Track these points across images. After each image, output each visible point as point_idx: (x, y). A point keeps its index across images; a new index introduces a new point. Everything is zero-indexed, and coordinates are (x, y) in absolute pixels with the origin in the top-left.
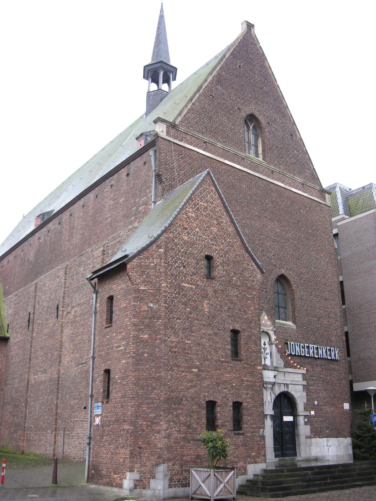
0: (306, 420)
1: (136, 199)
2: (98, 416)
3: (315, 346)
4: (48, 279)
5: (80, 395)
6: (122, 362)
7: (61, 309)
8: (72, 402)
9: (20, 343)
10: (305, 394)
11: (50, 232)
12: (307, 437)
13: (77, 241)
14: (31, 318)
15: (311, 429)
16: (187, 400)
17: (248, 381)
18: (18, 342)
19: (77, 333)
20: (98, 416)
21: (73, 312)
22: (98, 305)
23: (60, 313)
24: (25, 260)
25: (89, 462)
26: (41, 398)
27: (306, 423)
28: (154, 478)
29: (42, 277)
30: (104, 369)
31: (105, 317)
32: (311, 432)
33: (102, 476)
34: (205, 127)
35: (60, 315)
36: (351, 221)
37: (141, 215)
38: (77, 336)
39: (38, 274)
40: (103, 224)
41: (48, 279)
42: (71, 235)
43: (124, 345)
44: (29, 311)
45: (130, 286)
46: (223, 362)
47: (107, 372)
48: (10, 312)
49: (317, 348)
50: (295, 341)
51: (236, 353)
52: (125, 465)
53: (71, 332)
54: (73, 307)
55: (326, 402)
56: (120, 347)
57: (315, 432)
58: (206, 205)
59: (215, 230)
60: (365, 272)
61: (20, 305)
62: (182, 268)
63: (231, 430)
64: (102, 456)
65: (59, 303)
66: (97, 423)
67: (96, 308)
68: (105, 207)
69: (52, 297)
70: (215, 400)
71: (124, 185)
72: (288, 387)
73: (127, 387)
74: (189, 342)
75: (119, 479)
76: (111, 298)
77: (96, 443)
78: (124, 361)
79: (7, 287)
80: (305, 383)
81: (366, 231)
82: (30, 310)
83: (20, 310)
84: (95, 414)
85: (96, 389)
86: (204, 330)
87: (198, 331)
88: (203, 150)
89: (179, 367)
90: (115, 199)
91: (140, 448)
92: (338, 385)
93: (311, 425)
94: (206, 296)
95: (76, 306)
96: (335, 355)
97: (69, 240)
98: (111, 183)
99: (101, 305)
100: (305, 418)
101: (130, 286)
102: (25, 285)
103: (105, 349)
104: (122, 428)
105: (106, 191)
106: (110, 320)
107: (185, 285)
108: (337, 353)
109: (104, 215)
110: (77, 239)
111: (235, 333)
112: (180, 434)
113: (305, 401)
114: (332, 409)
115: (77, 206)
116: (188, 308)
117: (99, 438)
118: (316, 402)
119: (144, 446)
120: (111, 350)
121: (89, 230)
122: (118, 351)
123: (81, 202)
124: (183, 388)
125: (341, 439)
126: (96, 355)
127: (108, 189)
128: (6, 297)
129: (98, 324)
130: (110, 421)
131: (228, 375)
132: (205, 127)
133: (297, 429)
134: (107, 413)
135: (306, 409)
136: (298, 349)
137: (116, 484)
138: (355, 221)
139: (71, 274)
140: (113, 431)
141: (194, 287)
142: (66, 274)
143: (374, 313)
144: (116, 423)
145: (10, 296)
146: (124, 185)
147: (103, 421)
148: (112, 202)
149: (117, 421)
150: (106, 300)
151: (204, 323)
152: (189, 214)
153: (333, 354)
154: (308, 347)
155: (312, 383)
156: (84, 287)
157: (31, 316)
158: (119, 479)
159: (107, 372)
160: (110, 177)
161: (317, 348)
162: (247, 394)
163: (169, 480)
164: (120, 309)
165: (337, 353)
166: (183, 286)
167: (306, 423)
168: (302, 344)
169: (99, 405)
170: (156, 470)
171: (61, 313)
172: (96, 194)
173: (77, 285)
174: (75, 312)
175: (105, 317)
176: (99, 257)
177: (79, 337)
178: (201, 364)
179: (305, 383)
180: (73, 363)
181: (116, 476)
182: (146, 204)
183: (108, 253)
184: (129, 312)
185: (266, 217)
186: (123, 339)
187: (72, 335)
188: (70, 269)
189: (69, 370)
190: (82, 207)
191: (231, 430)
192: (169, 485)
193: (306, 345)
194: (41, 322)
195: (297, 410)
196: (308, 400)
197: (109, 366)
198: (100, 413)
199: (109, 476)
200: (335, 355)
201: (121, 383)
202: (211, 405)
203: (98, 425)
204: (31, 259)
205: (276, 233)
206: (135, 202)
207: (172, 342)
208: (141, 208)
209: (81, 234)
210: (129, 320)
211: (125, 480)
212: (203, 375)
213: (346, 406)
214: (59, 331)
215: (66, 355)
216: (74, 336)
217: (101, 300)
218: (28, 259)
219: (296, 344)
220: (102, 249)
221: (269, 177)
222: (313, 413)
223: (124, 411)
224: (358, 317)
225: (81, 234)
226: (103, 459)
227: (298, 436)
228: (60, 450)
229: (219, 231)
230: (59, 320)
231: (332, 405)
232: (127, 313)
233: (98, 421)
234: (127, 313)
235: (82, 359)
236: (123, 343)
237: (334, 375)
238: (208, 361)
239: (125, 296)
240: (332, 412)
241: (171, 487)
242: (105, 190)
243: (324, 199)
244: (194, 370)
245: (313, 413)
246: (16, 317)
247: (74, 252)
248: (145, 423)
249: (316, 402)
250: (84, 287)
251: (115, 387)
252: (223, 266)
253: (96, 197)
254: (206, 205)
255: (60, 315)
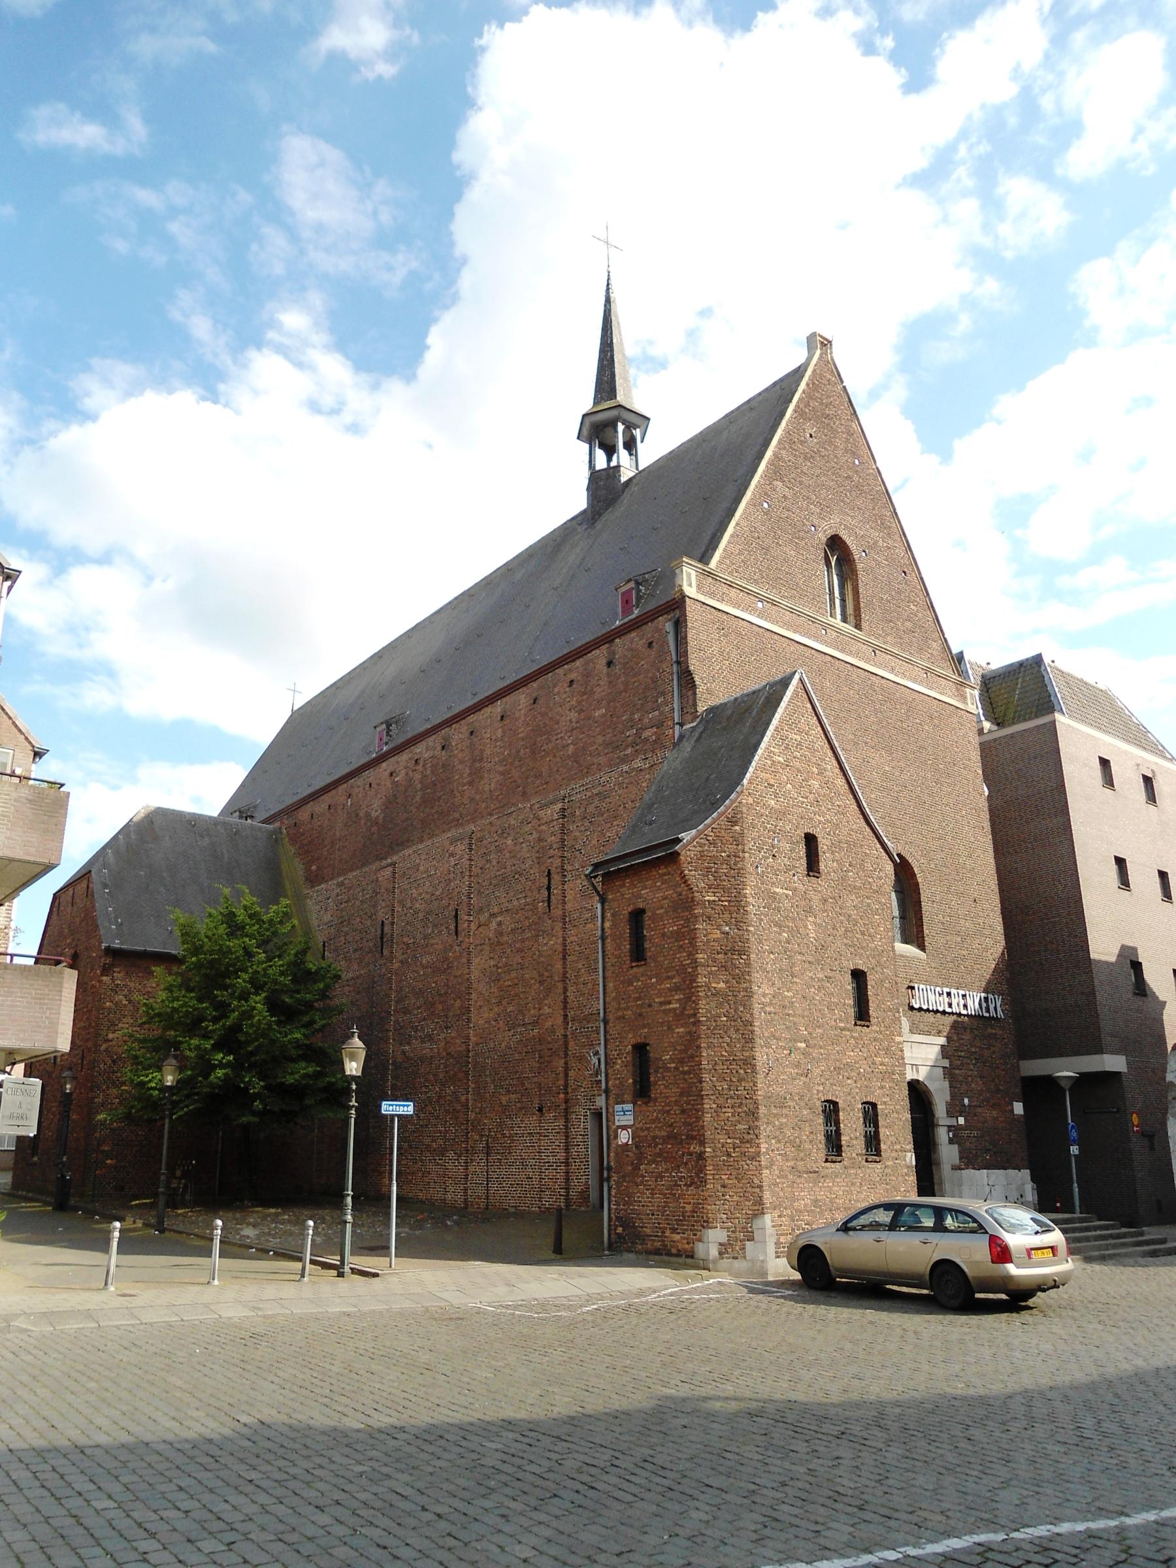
0: (951, 1135)
1: (633, 714)
2: (624, 1128)
3: (962, 992)
4: (423, 857)
5: (523, 1085)
6: (677, 1030)
7: (466, 917)
8: (504, 1100)
9: (359, 981)
10: (947, 1084)
11: (421, 763)
12: (955, 1168)
13: (493, 785)
14: (385, 932)
15: (960, 1152)
16: (792, 1099)
17: (882, 1064)
18: (353, 979)
19: (506, 965)
20: (624, 1128)
21: (493, 925)
22: (607, 924)
23: (463, 926)
24: (357, 815)
25: (609, 1214)
26: (424, 1089)
27: (951, 1141)
28: (751, 1239)
29: (407, 852)
30: (633, 1041)
31: (627, 947)
32: (961, 1158)
33: (643, 1238)
34: (760, 570)
35: (464, 930)
36: (1004, 737)
37: (648, 746)
38: (509, 972)
39: (399, 844)
40: (555, 756)
41: (423, 857)
42: (476, 775)
43: (679, 1000)
44: (380, 919)
45: (684, 893)
46: (842, 1029)
47: (641, 1049)
48: (327, 918)
49: (964, 996)
50: (926, 982)
51: (862, 1014)
52: (698, 1216)
53: (492, 963)
54: (493, 915)
55: (983, 1101)
56: (670, 1003)
57: (967, 1158)
58: (798, 737)
59: (815, 784)
60: (1035, 840)
61: (353, 905)
62: (771, 860)
63: (861, 1155)
64: (640, 1202)
65: (458, 905)
66: (625, 1141)
67: (603, 929)
68: (558, 723)
69: (438, 893)
70: (834, 1099)
71: (601, 683)
72: (917, 1071)
73: (692, 1076)
74: (790, 994)
75: (685, 1241)
76: (637, 916)
77: (624, 1177)
78: (681, 1030)
79: (314, 868)
80: (946, 1063)
81: (1035, 758)
82: (381, 914)
83: (353, 914)
84: (617, 1123)
85: (615, 1079)
86: (810, 971)
87: (802, 974)
88: (758, 616)
89: (778, 1039)
90: (582, 711)
91: (724, 1186)
92: (1003, 1067)
93: (960, 1145)
94: (809, 911)
95: (501, 913)
96: (995, 1008)
97: (470, 783)
98: (573, 676)
99: (614, 925)
100: (949, 1131)
101: (684, 893)
102: (363, 865)
103: (632, 1006)
104: (686, 1150)
105: (558, 693)
106: (638, 954)
107: (778, 890)
108: (998, 1004)
109: (557, 739)
110: (490, 783)
111: (858, 976)
112: (787, 1160)
113: (948, 1098)
114: (994, 1113)
115: (486, 715)
116: (784, 931)
117: (630, 1168)
118: (966, 1101)
119: (731, 1182)
120: (649, 1009)
121: (521, 766)
122: (666, 1012)
123: (498, 707)
124: (785, 1077)
125: (1012, 1172)
126: (611, 1017)
127: (562, 687)
128: (312, 887)
129: (611, 960)
130: (654, 1138)
131: (852, 1054)
132: (760, 570)
133: (935, 1153)
134: (646, 1123)
135: (950, 1114)
136: (932, 997)
137: (679, 1251)
138: (1012, 736)
139: (483, 850)
140: (665, 1155)
141: (790, 893)
142: (471, 849)
143: (1055, 922)
144: (671, 1141)
145: (323, 886)
146: (601, 683)
147: (639, 1137)
148: (573, 715)
149: (671, 1137)
150: (627, 916)
151: (810, 959)
152: (776, 758)
153: (992, 1007)
154: (949, 994)
155: (959, 1062)
156: (517, 876)
157: (386, 928)
158: (685, 1241)
159: (641, 1049)
160: (567, 664)
161: (964, 996)
162: (882, 1087)
163: (775, 1244)
164: (664, 935)
165: (998, 1004)
166: (775, 893)
167: (951, 1141)
168: (938, 989)
169: (627, 1109)
170: (754, 1227)
171: (465, 925)
172: (534, 695)
173: (500, 873)
174: (500, 924)
175: (628, 946)
176: (553, 820)
177: (514, 974)
178: (810, 1034)
179: (946, 1063)
180: (501, 1022)
181: (677, 1237)
182: (660, 725)
183: (573, 814)
184: (687, 941)
185: (866, 743)
186: (677, 989)
187: (495, 969)
188: (480, 840)
189: (492, 1036)
190: (499, 718)
191: (861, 1155)
192: (776, 1252)
193: (946, 990)
194: (412, 941)
195: (933, 1116)
196: (953, 1096)
197: (645, 1037)
198: (631, 1123)
199: (661, 1236)
200: (995, 1008)
201: (676, 1068)
202: (831, 1111)
203: (626, 1144)
204: (374, 814)
205: (885, 772)
206: (631, 720)
207: (764, 995)
208: (646, 734)
209: (502, 773)
210: (688, 956)
211: (701, 1244)
212: (815, 1053)
213: (1018, 1108)
214: (464, 960)
215: (481, 1006)
216: (500, 970)
217: (613, 915)
218: (368, 815)
219: (928, 987)
220: (560, 805)
221: (867, 661)
222: (961, 1121)
223: (688, 1120)
224: (1020, 930)
225: (502, 773)
226: (643, 1206)
227: (938, 1164)
228: (481, 1191)
229: (823, 788)
230: (460, 939)
231: (993, 1106)
232: (681, 943)
233: (624, 1137)
234: (681, 943)
235: (524, 1015)
236: (676, 997)
237: (994, 1049)
238: (819, 1027)
239: (675, 911)
240: (995, 1119)
241: (778, 1257)
242: (556, 690)
243: (963, 698)
244: (800, 1045)
245: (961, 1121)
246: (345, 929)
247: (487, 807)
248: (729, 1141)
249: (966, 1101)
250: (517, 876)
251: (664, 1077)
252: (833, 853)
253: (534, 703)
254: (798, 737)
255: (464, 930)
